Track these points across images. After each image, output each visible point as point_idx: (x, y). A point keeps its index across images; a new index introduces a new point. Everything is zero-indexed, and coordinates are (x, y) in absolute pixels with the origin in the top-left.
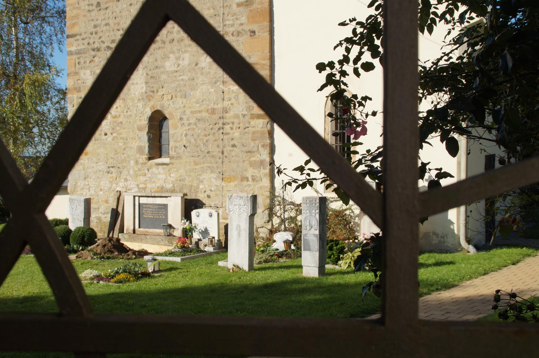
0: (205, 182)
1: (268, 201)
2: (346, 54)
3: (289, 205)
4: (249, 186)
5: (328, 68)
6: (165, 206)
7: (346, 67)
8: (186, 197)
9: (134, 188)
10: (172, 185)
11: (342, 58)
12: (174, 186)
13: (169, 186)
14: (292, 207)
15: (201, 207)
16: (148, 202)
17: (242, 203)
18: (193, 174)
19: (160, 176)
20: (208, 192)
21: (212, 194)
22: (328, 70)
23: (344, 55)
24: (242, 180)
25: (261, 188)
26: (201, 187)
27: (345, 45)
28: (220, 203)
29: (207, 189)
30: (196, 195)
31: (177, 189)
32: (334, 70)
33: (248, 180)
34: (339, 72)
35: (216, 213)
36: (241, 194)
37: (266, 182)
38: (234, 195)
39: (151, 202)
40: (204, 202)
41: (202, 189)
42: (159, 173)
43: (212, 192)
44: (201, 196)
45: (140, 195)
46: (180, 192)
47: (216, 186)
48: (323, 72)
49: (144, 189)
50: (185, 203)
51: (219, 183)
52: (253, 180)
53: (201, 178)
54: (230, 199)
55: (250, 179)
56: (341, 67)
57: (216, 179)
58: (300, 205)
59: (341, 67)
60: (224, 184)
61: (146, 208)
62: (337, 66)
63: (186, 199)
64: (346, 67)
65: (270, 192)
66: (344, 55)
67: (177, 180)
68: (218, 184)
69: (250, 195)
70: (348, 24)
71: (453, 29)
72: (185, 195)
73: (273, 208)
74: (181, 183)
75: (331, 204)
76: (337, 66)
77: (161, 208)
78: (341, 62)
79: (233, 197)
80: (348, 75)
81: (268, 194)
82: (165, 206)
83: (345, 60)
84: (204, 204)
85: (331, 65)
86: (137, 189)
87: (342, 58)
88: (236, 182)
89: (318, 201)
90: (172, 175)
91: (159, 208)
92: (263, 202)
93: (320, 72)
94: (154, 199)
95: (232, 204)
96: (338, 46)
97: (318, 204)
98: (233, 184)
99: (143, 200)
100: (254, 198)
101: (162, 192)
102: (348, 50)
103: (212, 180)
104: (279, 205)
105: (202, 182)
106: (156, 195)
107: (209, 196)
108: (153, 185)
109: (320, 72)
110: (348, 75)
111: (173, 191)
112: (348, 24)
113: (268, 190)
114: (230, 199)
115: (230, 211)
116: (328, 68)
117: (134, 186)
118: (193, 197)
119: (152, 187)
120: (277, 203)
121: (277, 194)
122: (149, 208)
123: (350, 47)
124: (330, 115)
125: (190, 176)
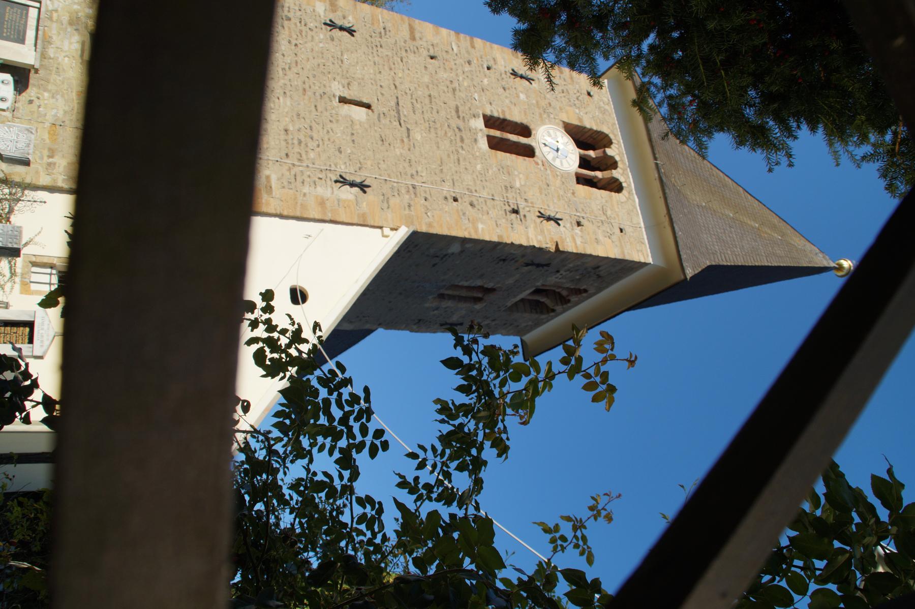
0: (52, 101)
1: (17, 179)
2: (278, 329)
3: (10, 206)
4: (42, 158)
5: (264, 304)
6: (21, 40)
7: (262, 327)
8: (33, 71)
9: (53, 4)
10: (52, 56)
11: (274, 323)
12: (50, 58)
13: (51, 52)
14: (7, 210)
15: (16, 89)
16: (29, 19)
17: (19, 145)
18: (66, 86)
19: (66, 43)
20: (37, 102)
21: (34, 107)
22: (260, 304)
23: (277, 326)
24: (50, 149)
25: (37, 172)
26: (46, 94)
27: (291, 328)
28: (20, 116)
29: (42, 102)
30: (34, 85)
31: (46, 62)
32: (261, 313)
33: (49, 157)
34: (256, 319)
35: (5, 108)
36: (32, 146)
37: (44, 180)
38: (33, 137)
39: (29, 23)
40: (24, 94)
41: (43, 95)
42: (71, 43)
43: (36, 107)
44: (31, 92)
45: (43, 10)
46: (41, 65)
47: (45, 115)
48: (261, 297)
49: (51, 19)
50: (24, 69)
51: (50, 118)
52: (49, 164)
53: (58, 97)
54: (28, 130)
55: (51, 160)
56: (262, 322)
57: (55, 115)
58: (8, 220)
59: (262, 322)
60: (47, 125)
61: (22, 14)
62: (266, 316)
63: (29, 71)
64: (262, 327)
65: (29, 184)
66: (277, 326)
67: (59, 64)
68: (47, 118)
69: (30, 157)
70: (314, 332)
71: (258, 441)
72: (37, 71)
73: (6, 185)
74: (55, 69)
75: (7, 262)
76: (266, 316)
77: (19, 34)
78: (268, 322)
79: (30, 134)
80: (252, 330)
81: (28, 180)
82: (21, 40)
83: (271, 328)
84: (20, 94)
85: (269, 309)
86: (50, 8)
87: (274, 323)
88: (48, 141)
89: (15, 246)
90: (66, 59)
91: (19, 31)
92: (18, 172)
93: (261, 294)
94: (34, 28)
95: (20, 131)
96: (291, 319)
97: (10, 246)
98: (46, 136)
99: (33, 13)
100: (26, 163)
101: (43, 41)
102: (284, 332)
103: (55, 111)
104: (10, 194)
105: (53, 97)
106: (40, 32)
107: (31, 102)
108: (54, 32)
109: (261, 294)
110: (252, 330)
111: (43, 56)
112: (314, 332)
113: (34, 182)
114: (28, 130)
115: (9, 127)
116: (264, 304)
117: (56, 6)
118: (31, 81)
119: (53, 30)
120: (14, 191)
121: (26, 192)
122: (21, 17)
123: (287, 335)
124: (66, 232)
125: (63, 83)
